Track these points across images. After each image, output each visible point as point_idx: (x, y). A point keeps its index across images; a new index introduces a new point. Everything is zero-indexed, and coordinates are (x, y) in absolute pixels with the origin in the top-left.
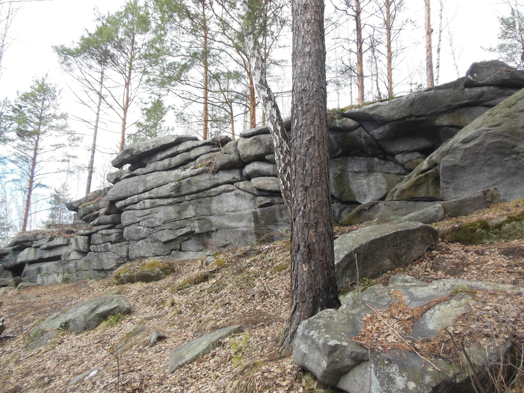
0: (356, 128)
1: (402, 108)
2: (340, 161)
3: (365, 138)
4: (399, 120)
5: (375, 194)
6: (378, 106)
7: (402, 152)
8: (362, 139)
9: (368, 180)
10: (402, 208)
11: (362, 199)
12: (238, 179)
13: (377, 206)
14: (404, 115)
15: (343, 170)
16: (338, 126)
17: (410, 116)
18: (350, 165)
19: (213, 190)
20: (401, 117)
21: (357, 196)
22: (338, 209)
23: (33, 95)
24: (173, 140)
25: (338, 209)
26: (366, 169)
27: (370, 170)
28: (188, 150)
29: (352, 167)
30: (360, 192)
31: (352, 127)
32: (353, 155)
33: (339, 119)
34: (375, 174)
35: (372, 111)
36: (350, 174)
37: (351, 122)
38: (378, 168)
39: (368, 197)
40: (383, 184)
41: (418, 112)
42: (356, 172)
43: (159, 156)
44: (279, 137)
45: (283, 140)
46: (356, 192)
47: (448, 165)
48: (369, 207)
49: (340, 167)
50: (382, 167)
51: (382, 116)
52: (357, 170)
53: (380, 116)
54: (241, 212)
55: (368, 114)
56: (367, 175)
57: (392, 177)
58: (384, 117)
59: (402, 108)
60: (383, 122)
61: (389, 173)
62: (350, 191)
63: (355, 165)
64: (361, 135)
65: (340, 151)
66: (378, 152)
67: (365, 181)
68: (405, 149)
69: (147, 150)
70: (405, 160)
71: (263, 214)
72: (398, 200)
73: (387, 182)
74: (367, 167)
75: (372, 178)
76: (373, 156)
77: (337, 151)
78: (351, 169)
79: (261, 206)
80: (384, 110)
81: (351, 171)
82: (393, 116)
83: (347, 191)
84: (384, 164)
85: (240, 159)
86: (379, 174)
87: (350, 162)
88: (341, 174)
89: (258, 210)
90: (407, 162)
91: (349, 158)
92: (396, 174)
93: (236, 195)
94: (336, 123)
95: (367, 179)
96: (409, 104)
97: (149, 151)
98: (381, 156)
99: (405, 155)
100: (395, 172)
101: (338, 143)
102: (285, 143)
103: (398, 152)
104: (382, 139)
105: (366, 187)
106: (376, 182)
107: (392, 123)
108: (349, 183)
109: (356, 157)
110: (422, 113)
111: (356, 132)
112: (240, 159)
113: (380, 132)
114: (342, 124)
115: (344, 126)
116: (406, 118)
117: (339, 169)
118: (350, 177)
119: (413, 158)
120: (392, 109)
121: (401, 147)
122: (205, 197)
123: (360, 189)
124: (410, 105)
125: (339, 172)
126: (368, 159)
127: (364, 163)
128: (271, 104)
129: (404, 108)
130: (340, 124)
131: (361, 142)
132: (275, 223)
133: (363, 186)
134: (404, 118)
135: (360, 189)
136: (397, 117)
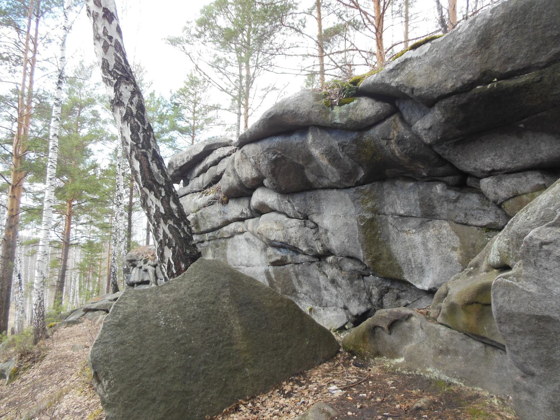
0: (378, 120)
1: (458, 59)
2: (370, 192)
3: (400, 141)
4: (456, 92)
5: (438, 269)
6: (406, 60)
7: (492, 173)
8: (393, 146)
9: (424, 237)
10: (456, 353)
11: (416, 277)
12: (247, 214)
13: (406, 324)
14: (467, 77)
15: (376, 211)
16: (338, 121)
17: (485, 77)
18: (389, 199)
19: (225, 228)
20: (459, 84)
21: (405, 269)
22: (377, 290)
23: (186, 90)
24: (201, 149)
25: (377, 290)
26: (419, 210)
27: (428, 214)
28: (216, 163)
29: (392, 205)
30: (410, 260)
31: (368, 119)
32: (394, 178)
33: (341, 104)
34: (437, 223)
35: (395, 77)
36: (390, 219)
37: (366, 107)
38: (443, 209)
39: (426, 274)
40: (454, 249)
41: (510, 60)
42: (401, 216)
43: (197, 170)
44: (139, 185)
45: (147, 191)
46: (403, 259)
47: (513, 308)
48: (388, 323)
49: (369, 205)
50: (451, 206)
51: (416, 86)
52: (402, 212)
53: (413, 89)
54: (254, 268)
55: (388, 86)
56: (422, 225)
57: (474, 235)
58: (421, 89)
59: (458, 59)
60: (428, 102)
61: (466, 224)
62: (391, 257)
63: (401, 200)
64: (391, 137)
65: (362, 174)
66: (441, 170)
67: (417, 238)
68: (500, 164)
69: (182, 164)
70: (503, 194)
71: (277, 274)
72: (446, 326)
73: (463, 246)
74: (421, 206)
75: (431, 232)
76: (432, 179)
77: (357, 173)
78: (391, 210)
79: (274, 264)
80: (418, 71)
81: (392, 214)
82: (440, 83)
83: (385, 256)
84: (456, 201)
85: (241, 184)
86: (446, 224)
87: (389, 194)
88: (372, 220)
89: (271, 269)
90: (507, 200)
91: (386, 185)
92: (482, 227)
93: (247, 240)
94: (334, 115)
95: (421, 234)
96: (474, 41)
97: (184, 165)
98: (450, 179)
99: (500, 180)
100: (479, 223)
101: (351, 156)
102: (152, 196)
103: (483, 172)
104: (437, 142)
105: (421, 252)
106: (439, 244)
107: (444, 102)
108: (388, 240)
109: (399, 183)
110: (520, 62)
111: (376, 132)
112: (241, 184)
113: (428, 125)
114: (345, 115)
115: (350, 120)
116: (471, 85)
117: (368, 210)
118: (391, 227)
119: (521, 190)
120: (437, 64)
121: (488, 160)
122: (220, 238)
123: (410, 256)
124: (479, 44)
125: (369, 216)
126: (421, 188)
127: (414, 197)
128: (121, 112)
129: (465, 57)
130: (341, 115)
131: (393, 152)
132: (294, 293)
133: (415, 247)
134: (470, 85)
135: (410, 256)
136: (449, 84)
